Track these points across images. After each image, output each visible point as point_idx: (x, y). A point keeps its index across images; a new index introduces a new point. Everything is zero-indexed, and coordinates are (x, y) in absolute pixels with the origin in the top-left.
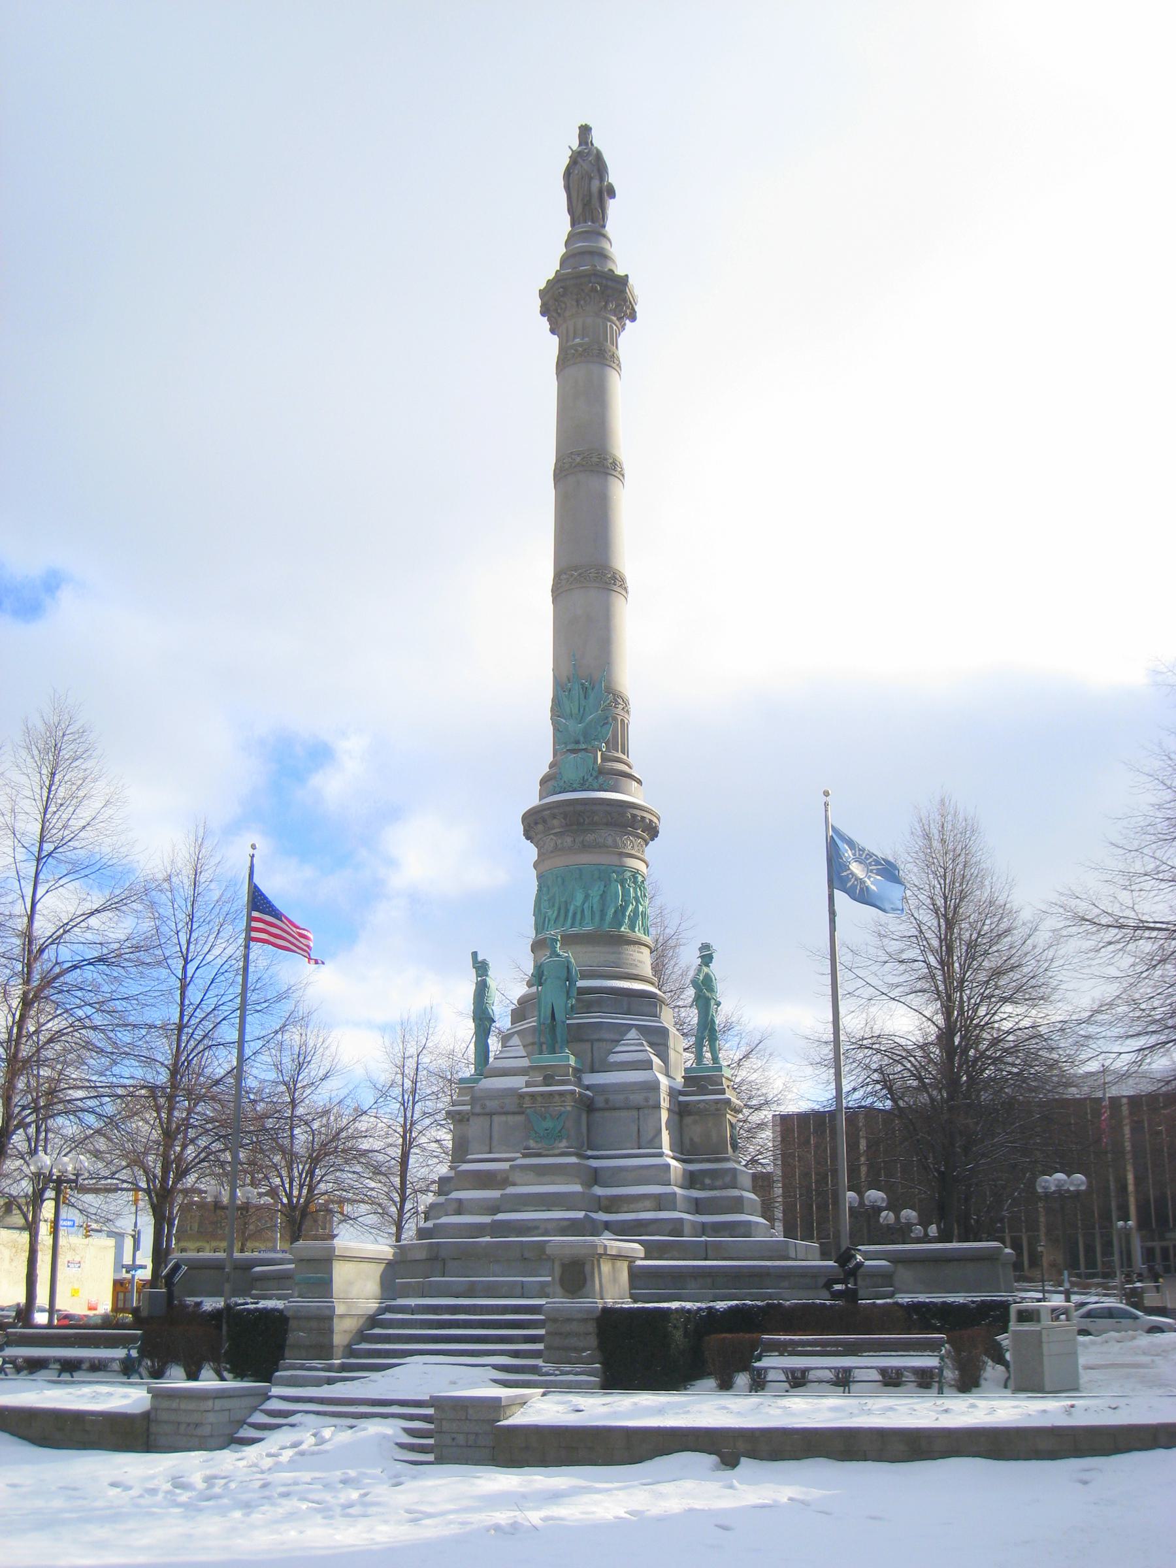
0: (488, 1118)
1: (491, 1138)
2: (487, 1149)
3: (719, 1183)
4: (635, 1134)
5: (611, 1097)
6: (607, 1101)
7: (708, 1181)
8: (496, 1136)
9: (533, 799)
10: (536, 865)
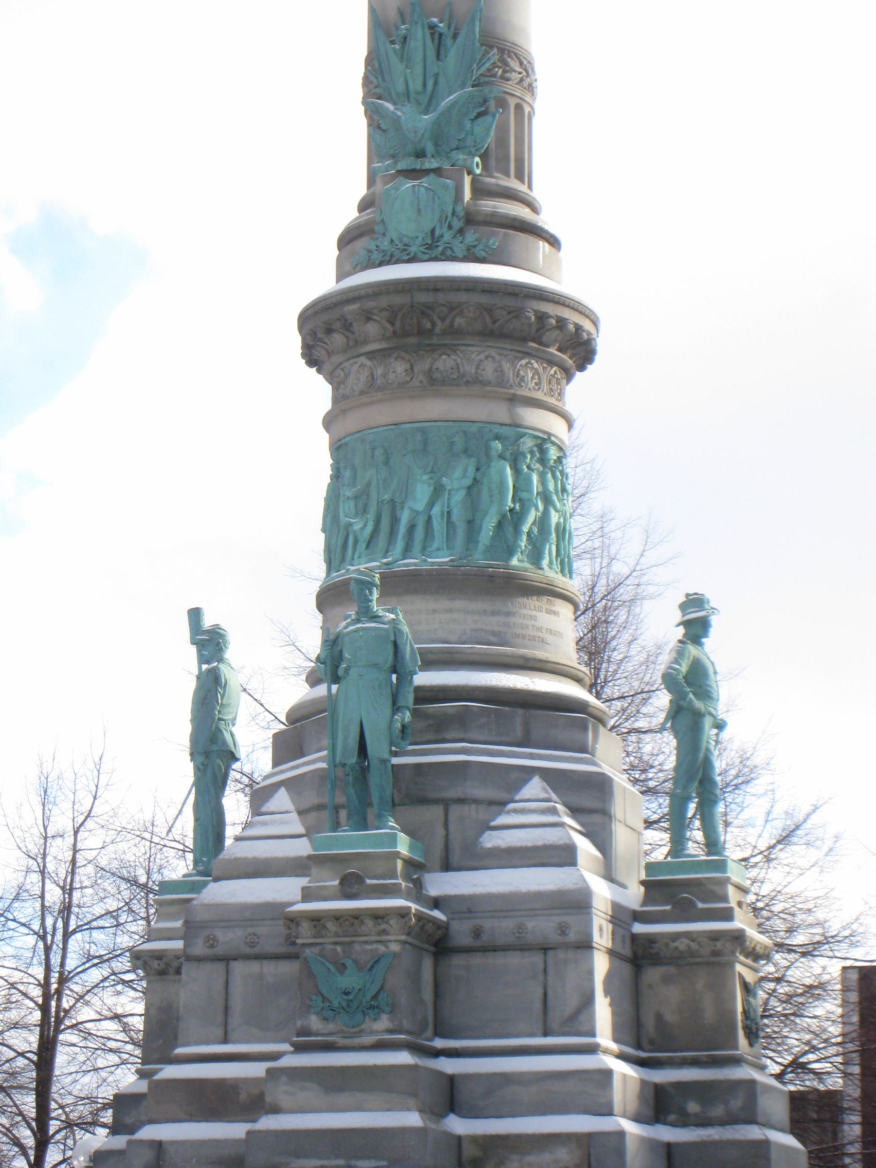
0: (220, 966)
1: (226, 1009)
2: (220, 1032)
3: (718, 1111)
4: (538, 1005)
5: (487, 924)
6: (477, 933)
7: (693, 1107)
8: (237, 1003)
9: (321, 278)
10: (329, 422)
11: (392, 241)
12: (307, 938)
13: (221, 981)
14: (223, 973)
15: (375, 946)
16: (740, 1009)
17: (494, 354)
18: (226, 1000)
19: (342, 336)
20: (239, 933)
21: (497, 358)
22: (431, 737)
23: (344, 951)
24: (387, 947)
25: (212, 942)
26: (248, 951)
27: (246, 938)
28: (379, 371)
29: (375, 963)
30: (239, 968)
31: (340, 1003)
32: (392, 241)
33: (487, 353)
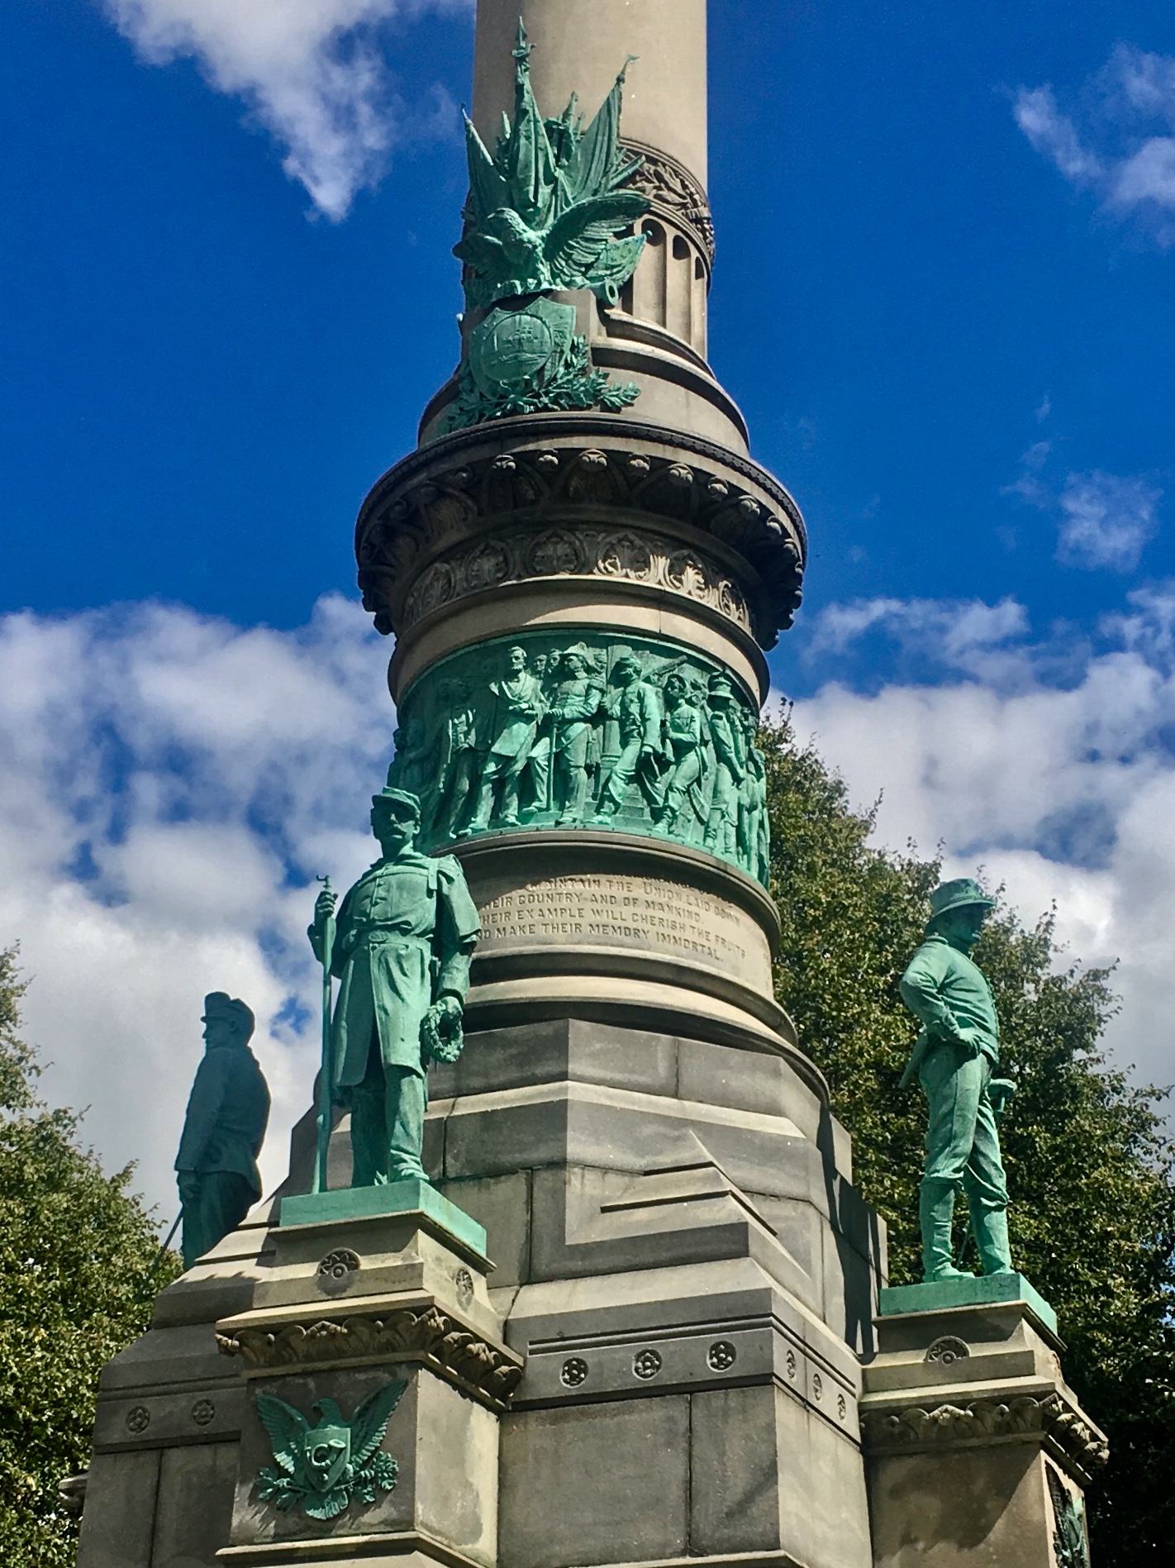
1: (154, 1530)
8: (170, 1518)
11: (482, 395)
12: (258, 1366)
13: (150, 1482)
14: (152, 1470)
15: (371, 1374)
16: (1051, 1527)
17: (632, 537)
18: (155, 1516)
19: (408, 540)
20: (183, 1401)
21: (638, 542)
22: (514, 1074)
23: (318, 1387)
24: (393, 1374)
25: (139, 1418)
26: (195, 1429)
27: (195, 1409)
28: (460, 574)
29: (370, 1402)
30: (177, 1458)
31: (306, 1478)
32: (482, 395)
33: (621, 535)
